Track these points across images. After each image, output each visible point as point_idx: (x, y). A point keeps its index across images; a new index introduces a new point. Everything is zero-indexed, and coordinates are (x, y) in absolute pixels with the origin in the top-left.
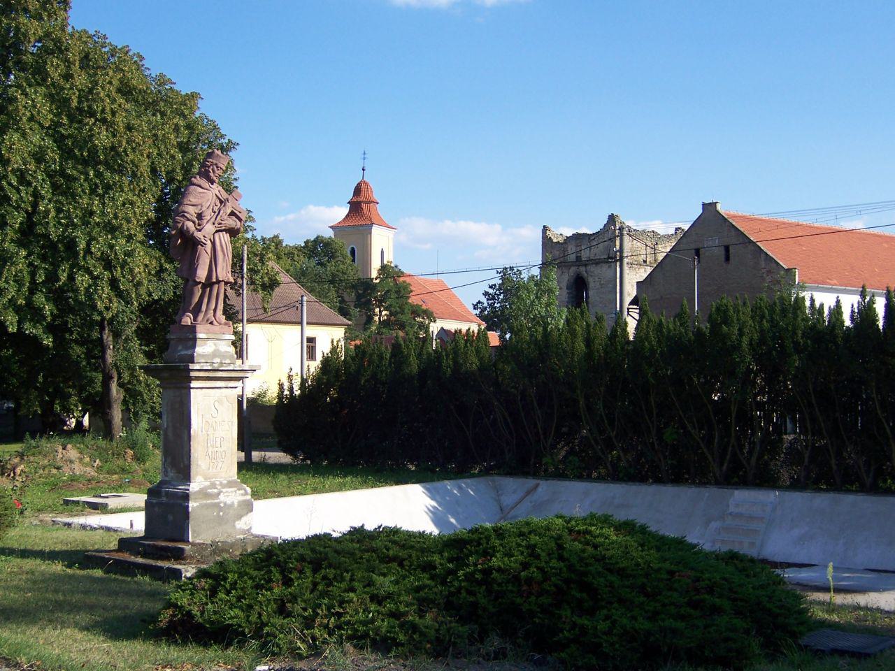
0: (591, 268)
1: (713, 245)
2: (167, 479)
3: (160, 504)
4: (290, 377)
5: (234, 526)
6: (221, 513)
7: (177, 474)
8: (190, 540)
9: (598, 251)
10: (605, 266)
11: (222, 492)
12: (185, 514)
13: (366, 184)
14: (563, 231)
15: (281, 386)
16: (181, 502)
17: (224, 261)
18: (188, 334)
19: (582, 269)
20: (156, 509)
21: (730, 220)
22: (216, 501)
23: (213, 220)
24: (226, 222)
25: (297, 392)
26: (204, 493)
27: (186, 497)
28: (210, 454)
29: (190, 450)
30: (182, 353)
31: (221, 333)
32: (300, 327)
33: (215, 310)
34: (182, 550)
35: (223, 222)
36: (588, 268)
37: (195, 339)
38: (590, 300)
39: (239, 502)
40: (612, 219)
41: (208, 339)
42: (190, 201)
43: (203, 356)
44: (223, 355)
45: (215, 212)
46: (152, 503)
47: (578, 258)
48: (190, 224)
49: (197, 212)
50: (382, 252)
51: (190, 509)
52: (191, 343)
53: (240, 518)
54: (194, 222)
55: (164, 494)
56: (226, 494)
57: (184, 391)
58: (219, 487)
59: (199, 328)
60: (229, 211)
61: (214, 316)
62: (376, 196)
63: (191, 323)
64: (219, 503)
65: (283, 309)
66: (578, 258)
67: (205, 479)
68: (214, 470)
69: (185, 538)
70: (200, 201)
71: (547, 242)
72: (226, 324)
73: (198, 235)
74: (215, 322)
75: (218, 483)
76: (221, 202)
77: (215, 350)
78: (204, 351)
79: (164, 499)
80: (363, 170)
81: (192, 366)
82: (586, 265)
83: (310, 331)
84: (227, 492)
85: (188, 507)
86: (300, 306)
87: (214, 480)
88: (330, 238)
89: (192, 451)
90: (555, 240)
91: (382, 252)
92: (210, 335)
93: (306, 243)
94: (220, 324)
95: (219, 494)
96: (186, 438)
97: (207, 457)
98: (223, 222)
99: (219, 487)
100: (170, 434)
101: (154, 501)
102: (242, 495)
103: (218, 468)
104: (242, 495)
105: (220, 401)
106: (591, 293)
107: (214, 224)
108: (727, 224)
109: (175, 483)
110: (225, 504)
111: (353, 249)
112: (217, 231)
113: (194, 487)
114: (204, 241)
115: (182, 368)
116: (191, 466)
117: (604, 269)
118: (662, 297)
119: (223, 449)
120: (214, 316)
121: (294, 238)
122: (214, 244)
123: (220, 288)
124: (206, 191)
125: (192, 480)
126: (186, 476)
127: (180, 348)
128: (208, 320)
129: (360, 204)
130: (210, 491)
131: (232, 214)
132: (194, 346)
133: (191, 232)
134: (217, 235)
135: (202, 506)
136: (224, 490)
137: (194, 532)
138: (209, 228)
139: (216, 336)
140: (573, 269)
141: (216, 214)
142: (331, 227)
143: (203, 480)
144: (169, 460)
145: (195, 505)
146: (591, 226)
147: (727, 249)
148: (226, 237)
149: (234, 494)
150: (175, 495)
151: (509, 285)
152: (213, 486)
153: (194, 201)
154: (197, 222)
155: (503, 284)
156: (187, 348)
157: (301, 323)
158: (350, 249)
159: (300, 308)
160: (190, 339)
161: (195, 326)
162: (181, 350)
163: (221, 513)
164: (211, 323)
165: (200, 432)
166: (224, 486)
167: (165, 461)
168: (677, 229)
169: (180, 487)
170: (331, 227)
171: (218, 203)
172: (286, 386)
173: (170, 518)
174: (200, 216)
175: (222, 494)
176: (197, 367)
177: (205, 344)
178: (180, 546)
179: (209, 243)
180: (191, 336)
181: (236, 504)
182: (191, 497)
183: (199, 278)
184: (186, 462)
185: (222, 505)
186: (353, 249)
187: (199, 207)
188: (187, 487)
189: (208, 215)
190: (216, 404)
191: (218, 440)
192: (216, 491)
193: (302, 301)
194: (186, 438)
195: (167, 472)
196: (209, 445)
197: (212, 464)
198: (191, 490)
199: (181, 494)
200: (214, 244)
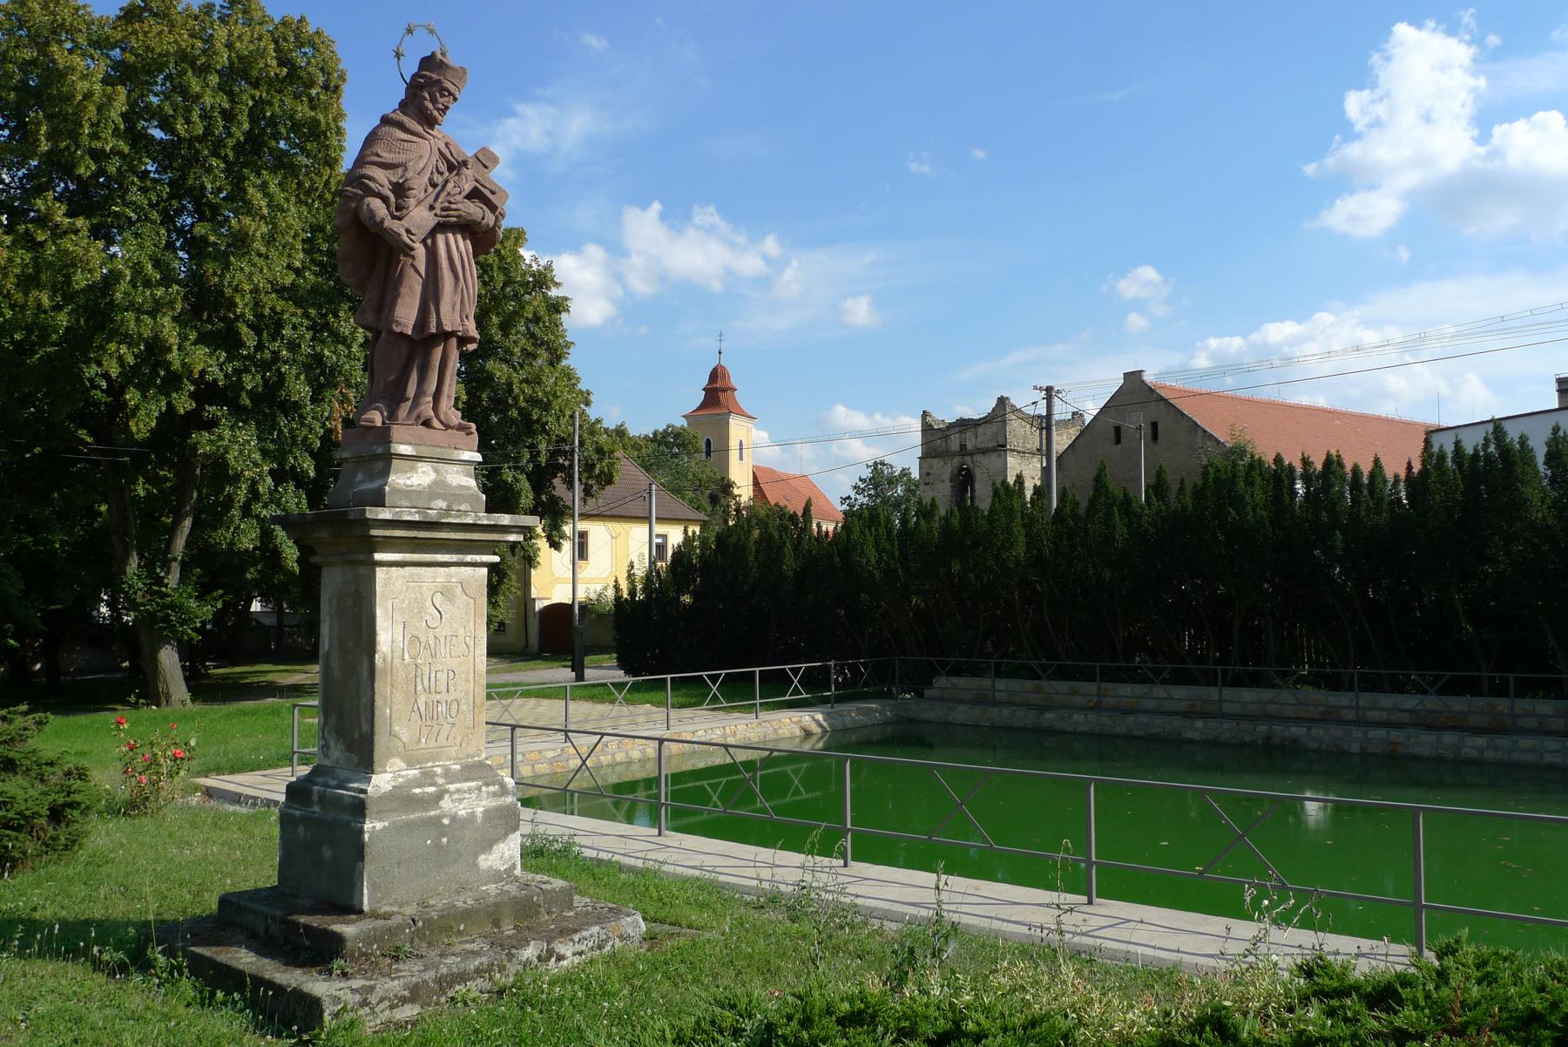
0: (978, 458)
1: (1136, 421)
2: (327, 762)
3: (308, 820)
4: (630, 576)
5: (476, 865)
6: (445, 840)
7: (348, 754)
8: (366, 908)
9: (984, 437)
10: (993, 456)
11: (447, 791)
12: (357, 849)
13: (722, 367)
14: (946, 414)
15: (617, 588)
16: (345, 817)
17: (455, 291)
18: (375, 447)
19: (968, 459)
20: (301, 830)
21: (1158, 391)
22: (433, 813)
23: (431, 200)
24: (460, 206)
25: (640, 596)
26: (402, 798)
27: (359, 809)
28: (422, 709)
29: (373, 701)
30: (364, 487)
31: (449, 446)
32: (648, 526)
33: (437, 397)
34: (338, 939)
35: (453, 206)
36: (975, 457)
37: (388, 457)
38: (976, 494)
39: (487, 812)
40: (1002, 401)
41: (418, 458)
42: (378, 155)
43: (407, 493)
44: (453, 495)
45: (434, 185)
46: (292, 816)
47: (963, 447)
48: (376, 204)
49: (394, 180)
50: (741, 459)
51: (366, 836)
52: (380, 464)
53: (491, 847)
54: (385, 200)
55: (315, 798)
56: (456, 796)
57: (362, 570)
58: (440, 781)
59: (396, 432)
60: (468, 188)
61: (435, 408)
62: (734, 382)
63: (383, 423)
64: (439, 818)
65: (627, 500)
66: (963, 447)
67: (408, 765)
68: (432, 744)
69: (355, 902)
70: (401, 158)
71: (927, 428)
72: (460, 428)
73: (398, 227)
74: (436, 423)
75: (439, 770)
76: (451, 168)
77: (435, 483)
78: (408, 482)
79: (317, 809)
80: (720, 353)
81: (373, 513)
82: (971, 455)
83: (659, 529)
84: (458, 791)
85: (361, 831)
86: (647, 496)
87: (430, 764)
88: (682, 428)
89: (378, 702)
90: (936, 427)
91: (741, 459)
92: (423, 448)
93: (655, 434)
94: (447, 427)
95: (439, 796)
96: (365, 674)
97: (416, 716)
98: (453, 206)
99: (440, 781)
100: (335, 664)
101: (297, 813)
102: (495, 795)
103: (442, 737)
104: (495, 795)
105: (446, 592)
106: (977, 486)
107: (432, 208)
108: (1155, 396)
109: (342, 774)
110: (454, 818)
111: (708, 440)
112: (441, 227)
113: (381, 782)
114: (408, 241)
115: (352, 517)
116: (376, 738)
117: (993, 458)
118: (1074, 485)
119: (453, 696)
120: (435, 408)
121: (642, 426)
122: (432, 254)
123: (449, 349)
124: (415, 138)
125: (377, 768)
126: (366, 763)
127: (359, 477)
128: (418, 417)
129: (717, 393)
130: (417, 791)
131: (475, 195)
132: (386, 472)
133: (378, 219)
134: (440, 238)
135: (395, 829)
136: (452, 787)
137: (374, 888)
138: (420, 217)
139: (438, 452)
140: (956, 460)
141: (439, 188)
142: (684, 416)
143: (403, 765)
144: (332, 721)
145: (379, 825)
146: (979, 408)
147: (1154, 426)
148: (460, 246)
149: (474, 796)
150: (338, 802)
151: (879, 478)
152: (427, 777)
153: (387, 157)
154: (392, 198)
155: (873, 478)
156: (371, 478)
157: (646, 519)
158: (705, 440)
159: (647, 499)
160: (376, 457)
161: (389, 428)
162: (361, 482)
163: (445, 840)
164: (427, 423)
165: (397, 661)
166: (449, 776)
167: (325, 723)
168: (1074, 413)
169: (355, 785)
170: (684, 416)
171: (443, 168)
172: (624, 585)
173: (327, 853)
174: (400, 190)
175: (447, 796)
176: (385, 514)
177: (413, 469)
178: (337, 928)
179: (420, 251)
180: (380, 451)
181: (479, 815)
182: (371, 809)
183: (399, 323)
184: (365, 728)
185: (446, 821)
186: (708, 440)
187: (400, 170)
188: (362, 787)
189: (419, 184)
190: (438, 599)
191: (442, 676)
192: (432, 789)
193: (650, 489)
194: (365, 674)
195: (328, 748)
196: (420, 688)
197: (425, 730)
198: (370, 789)
199: (347, 801)
200: (432, 254)
